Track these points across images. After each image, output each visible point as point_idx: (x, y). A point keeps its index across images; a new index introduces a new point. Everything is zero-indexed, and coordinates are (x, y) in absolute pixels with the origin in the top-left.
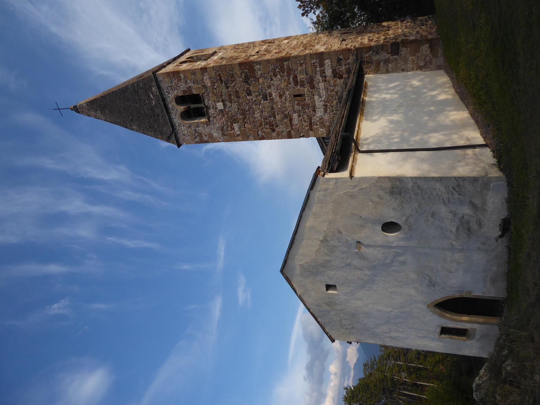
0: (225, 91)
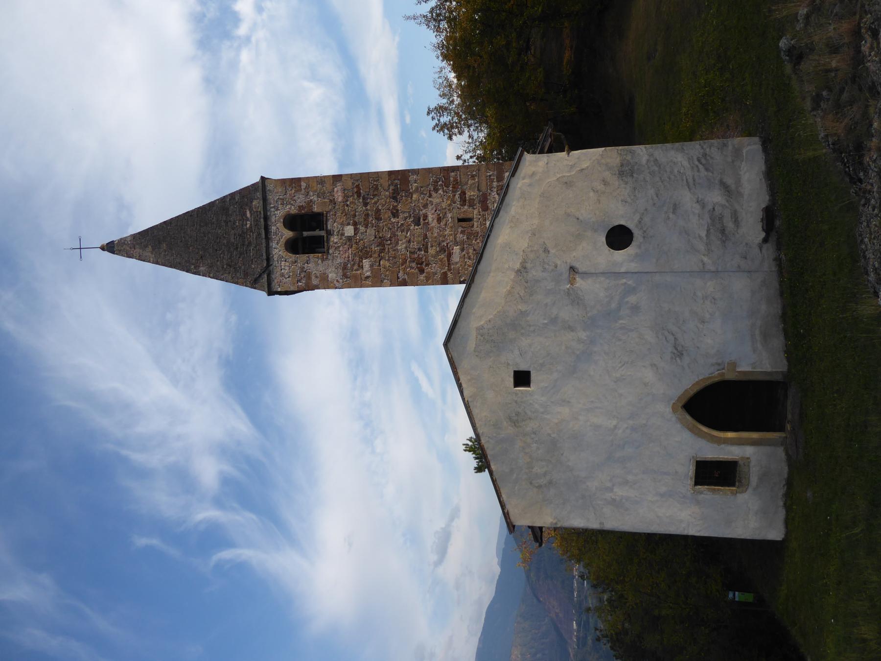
0: (360, 208)
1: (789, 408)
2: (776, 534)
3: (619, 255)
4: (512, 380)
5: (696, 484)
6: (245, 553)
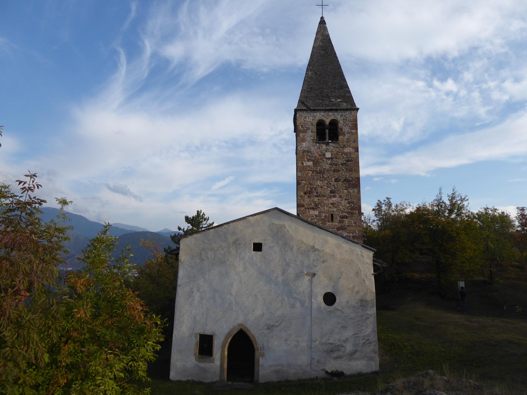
1: (240, 383)
2: (173, 375)
3: (321, 299)
4: (257, 242)
5: (200, 335)
6: (123, 69)
